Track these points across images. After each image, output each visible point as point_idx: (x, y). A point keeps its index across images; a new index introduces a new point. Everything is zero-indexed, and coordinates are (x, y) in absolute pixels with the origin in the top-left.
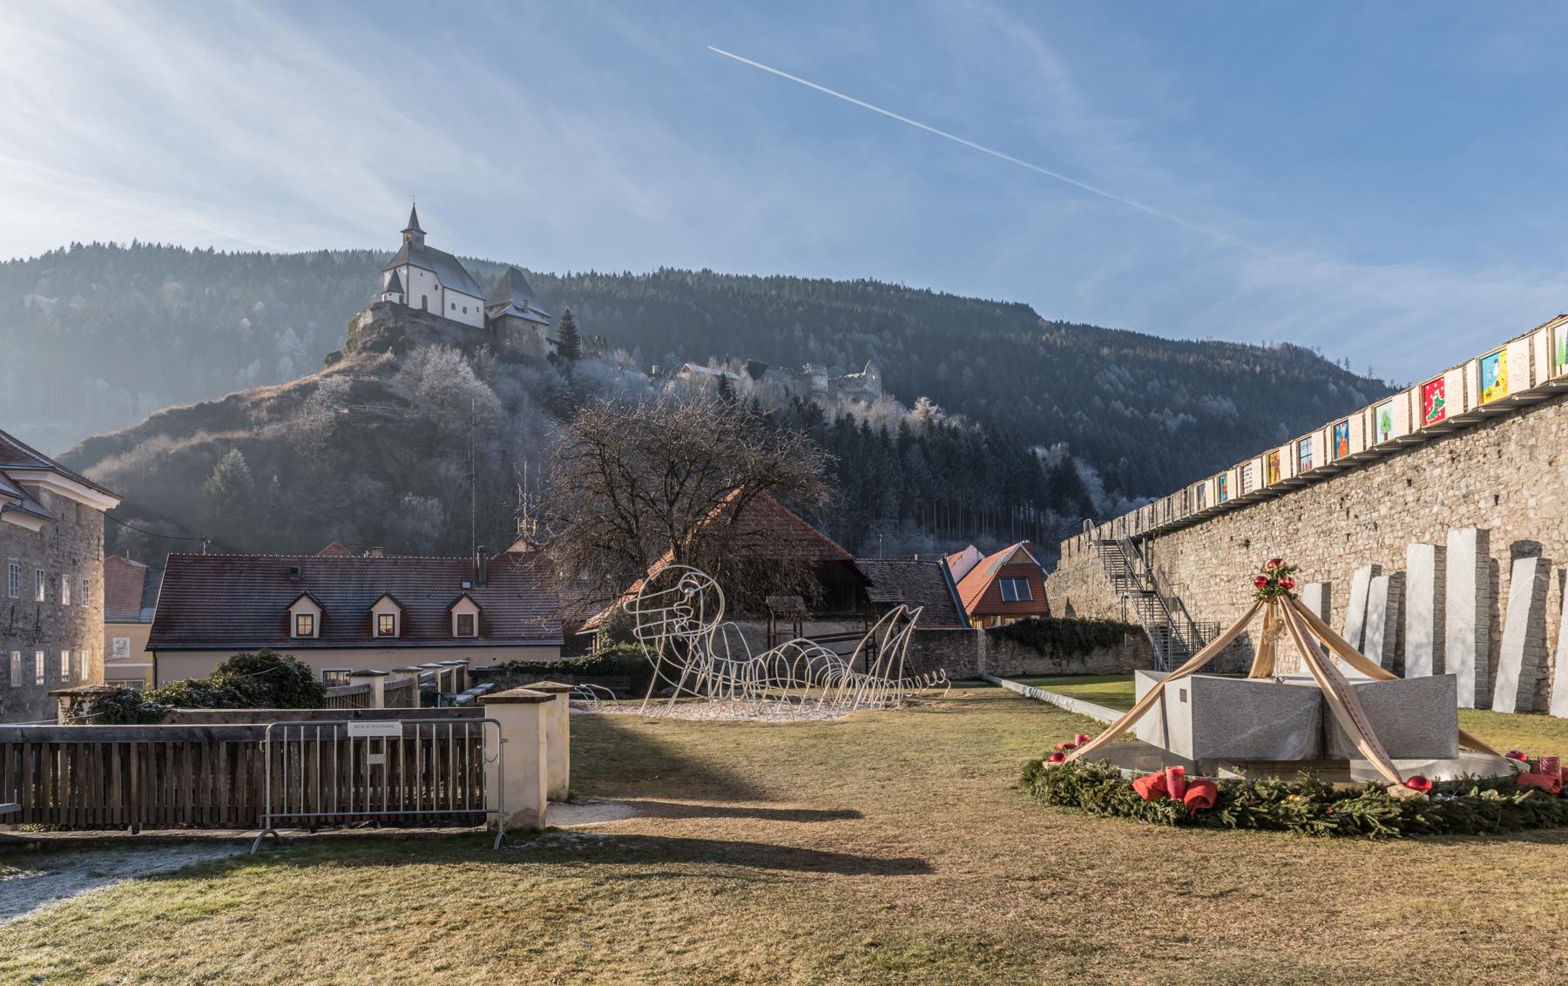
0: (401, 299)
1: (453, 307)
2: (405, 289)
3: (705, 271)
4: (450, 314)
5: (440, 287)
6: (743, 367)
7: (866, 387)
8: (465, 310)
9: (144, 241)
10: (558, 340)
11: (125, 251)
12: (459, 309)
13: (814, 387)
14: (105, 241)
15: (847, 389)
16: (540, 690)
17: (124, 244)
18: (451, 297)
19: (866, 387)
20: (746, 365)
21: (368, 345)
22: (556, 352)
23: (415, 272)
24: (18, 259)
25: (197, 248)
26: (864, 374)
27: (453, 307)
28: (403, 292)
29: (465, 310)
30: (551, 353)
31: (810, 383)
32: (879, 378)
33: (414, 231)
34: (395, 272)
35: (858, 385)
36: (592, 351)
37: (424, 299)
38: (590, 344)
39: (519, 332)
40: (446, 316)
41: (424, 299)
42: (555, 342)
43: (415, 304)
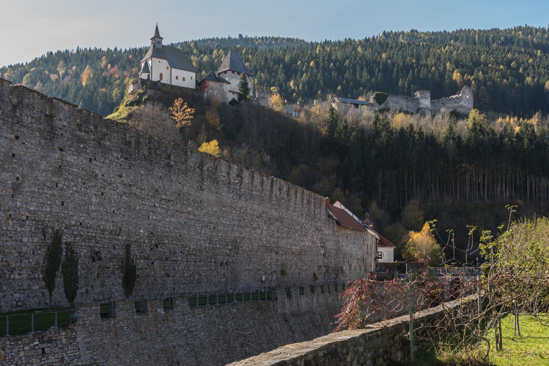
0: (149, 76)
1: (177, 78)
2: (150, 70)
3: (413, 31)
4: (175, 83)
5: (169, 68)
6: (372, 97)
7: (462, 103)
8: (184, 79)
9: (82, 47)
10: (239, 91)
11: (45, 59)
12: (180, 79)
13: (421, 106)
14: (62, 50)
15: (448, 105)
16: (369, 328)
17: (73, 50)
18: (176, 72)
19: (462, 103)
20: (374, 96)
21: (128, 103)
22: (236, 99)
23: (156, 60)
24: (113, 49)
25: (109, 49)
26: (460, 95)
27: (177, 78)
28: (149, 73)
29: (184, 79)
30: (234, 100)
31: (419, 103)
32: (472, 97)
33: (157, 38)
34: (146, 61)
35: (456, 102)
36: (262, 96)
37: (161, 75)
38: (261, 92)
39: (212, 89)
40: (173, 84)
41: (161, 75)
42: (236, 93)
43: (155, 78)
